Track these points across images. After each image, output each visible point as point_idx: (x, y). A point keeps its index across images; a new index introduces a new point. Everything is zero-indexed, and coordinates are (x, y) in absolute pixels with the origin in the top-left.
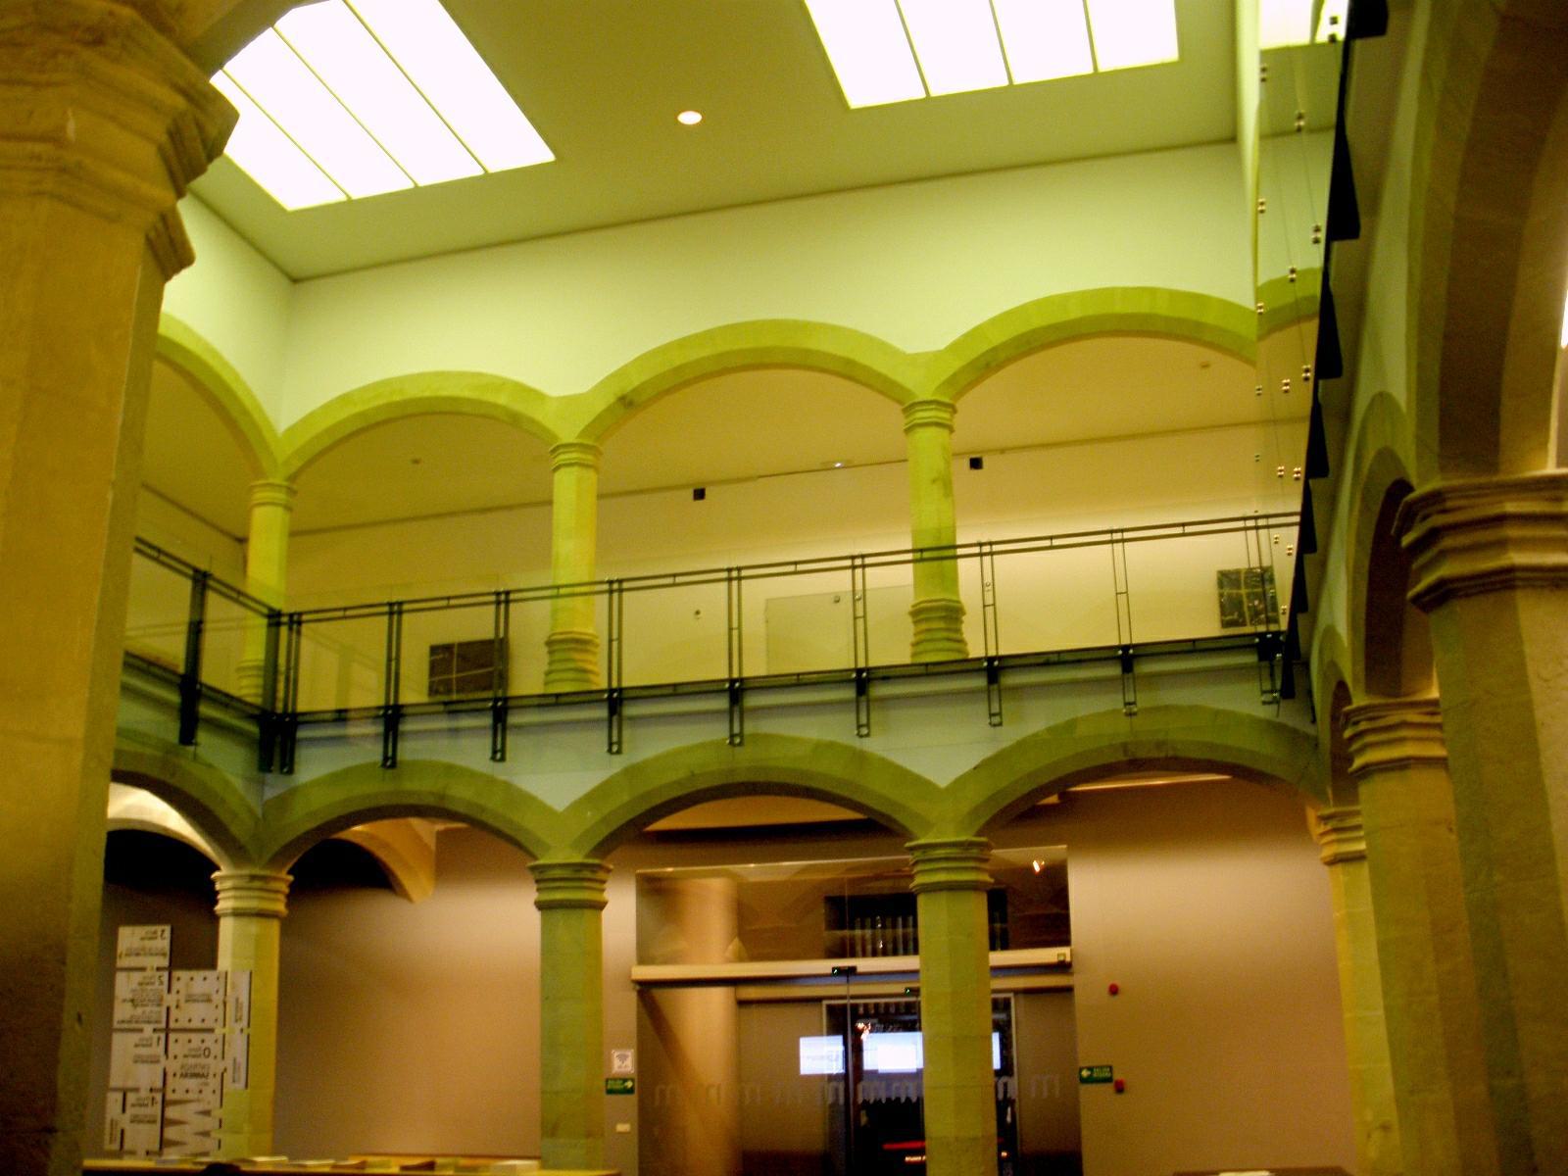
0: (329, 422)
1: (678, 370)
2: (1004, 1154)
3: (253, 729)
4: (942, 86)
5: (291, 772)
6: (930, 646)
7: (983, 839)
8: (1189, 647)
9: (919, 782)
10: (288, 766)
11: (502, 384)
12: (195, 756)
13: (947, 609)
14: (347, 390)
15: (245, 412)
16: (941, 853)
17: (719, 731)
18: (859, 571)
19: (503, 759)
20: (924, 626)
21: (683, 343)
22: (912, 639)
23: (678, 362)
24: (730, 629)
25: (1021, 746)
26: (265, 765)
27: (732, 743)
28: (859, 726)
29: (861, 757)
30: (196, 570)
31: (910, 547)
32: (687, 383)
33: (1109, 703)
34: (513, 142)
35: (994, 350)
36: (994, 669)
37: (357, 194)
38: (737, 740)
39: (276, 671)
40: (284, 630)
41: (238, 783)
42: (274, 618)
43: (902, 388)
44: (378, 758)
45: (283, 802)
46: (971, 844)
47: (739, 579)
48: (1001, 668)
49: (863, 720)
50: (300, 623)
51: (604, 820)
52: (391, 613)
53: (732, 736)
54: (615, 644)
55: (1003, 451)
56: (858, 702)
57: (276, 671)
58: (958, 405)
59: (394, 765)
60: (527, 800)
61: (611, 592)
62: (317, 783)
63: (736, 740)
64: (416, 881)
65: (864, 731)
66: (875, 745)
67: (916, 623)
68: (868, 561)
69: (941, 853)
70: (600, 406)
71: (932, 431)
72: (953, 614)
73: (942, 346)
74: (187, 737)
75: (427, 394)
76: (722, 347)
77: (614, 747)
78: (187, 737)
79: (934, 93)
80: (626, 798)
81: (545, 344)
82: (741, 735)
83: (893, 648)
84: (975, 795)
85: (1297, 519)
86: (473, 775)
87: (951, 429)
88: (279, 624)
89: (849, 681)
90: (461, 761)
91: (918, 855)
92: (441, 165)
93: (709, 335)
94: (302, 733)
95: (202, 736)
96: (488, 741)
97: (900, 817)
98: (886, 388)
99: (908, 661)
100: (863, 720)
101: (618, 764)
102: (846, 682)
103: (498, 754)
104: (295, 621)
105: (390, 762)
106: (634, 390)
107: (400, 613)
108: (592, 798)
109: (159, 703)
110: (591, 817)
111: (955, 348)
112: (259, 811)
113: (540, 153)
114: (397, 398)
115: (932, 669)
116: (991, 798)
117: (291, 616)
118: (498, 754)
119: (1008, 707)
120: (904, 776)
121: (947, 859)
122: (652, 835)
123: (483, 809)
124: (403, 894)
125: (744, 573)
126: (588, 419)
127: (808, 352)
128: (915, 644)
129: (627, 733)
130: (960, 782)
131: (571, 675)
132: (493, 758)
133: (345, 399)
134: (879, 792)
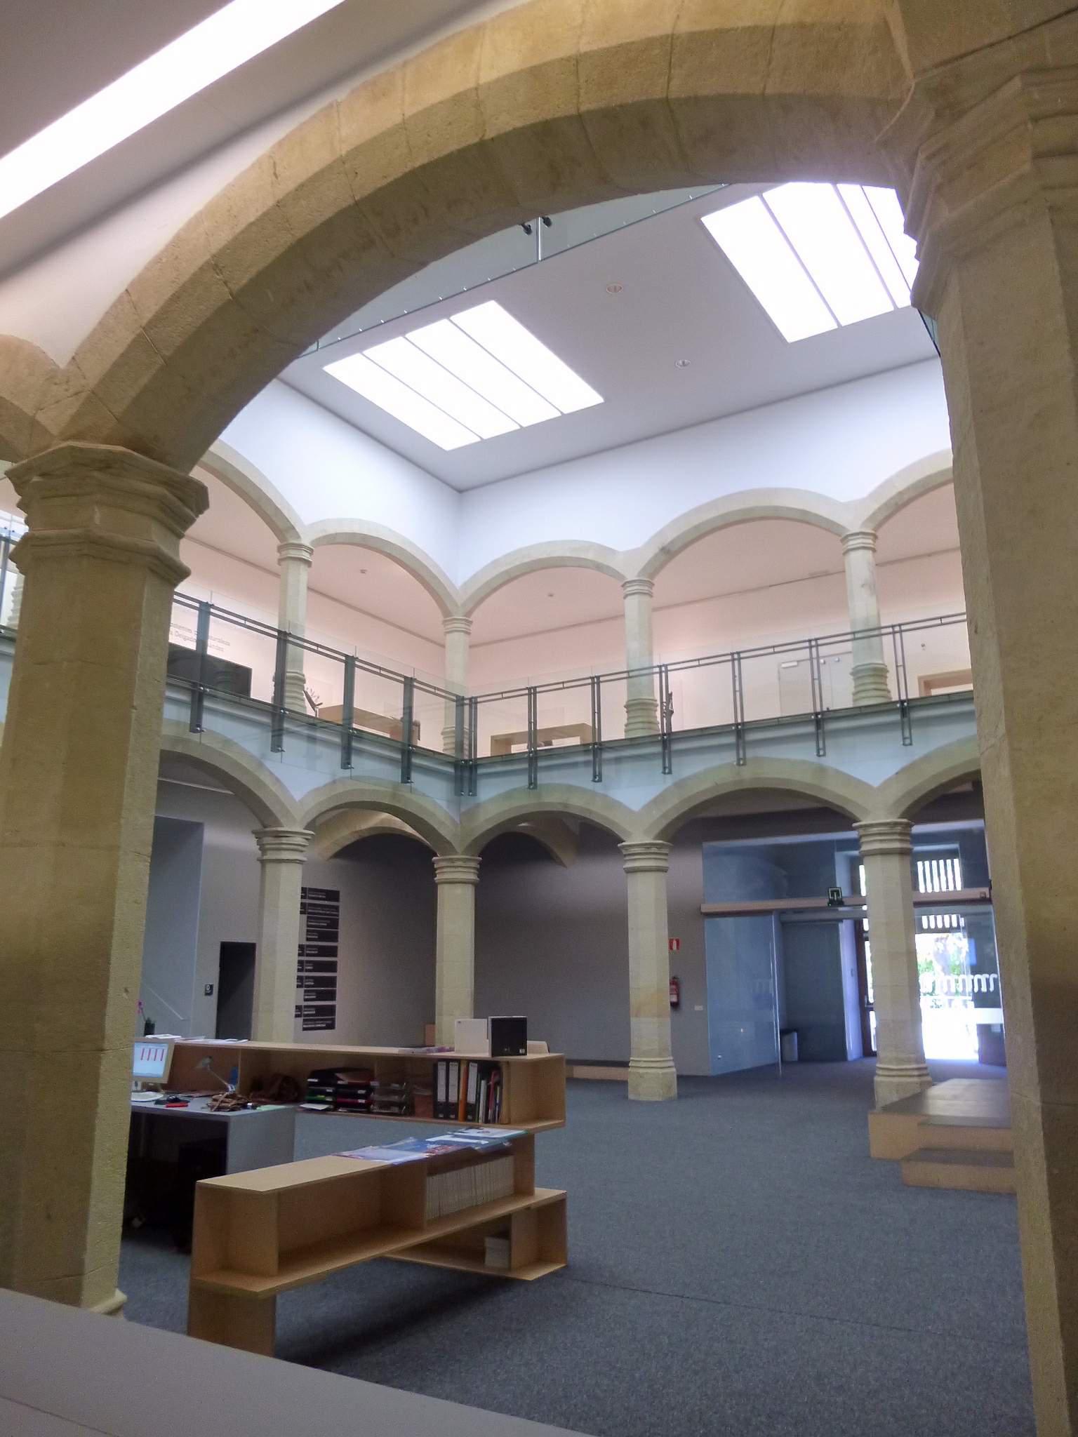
0: (485, 580)
1: (696, 527)
2: (698, 1008)
3: (451, 770)
4: (849, 317)
5: (475, 795)
6: (863, 694)
7: (905, 820)
8: (946, 699)
9: (859, 784)
10: (473, 791)
11: (590, 546)
12: (411, 790)
13: (875, 669)
14: (496, 557)
15: (435, 577)
16: (875, 830)
17: (522, 781)
18: (898, 636)
19: (600, 780)
20: (860, 682)
21: (698, 510)
22: (853, 690)
23: (696, 523)
24: (813, 679)
25: (927, 758)
26: (458, 791)
27: (739, 764)
28: (904, 739)
29: (822, 770)
30: (406, 678)
31: (849, 630)
32: (753, 520)
33: (730, 757)
34: (573, 393)
35: (900, 493)
36: (906, 708)
37: (567, 410)
38: (908, 741)
39: (463, 734)
40: (467, 708)
41: (443, 804)
42: (460, 701)
43: (839, 525)
44: (527, 783)
45: (469, 815)
46: (896, 824)
47: (901, 631)
48: (823, 720)
49: (907, 734)
50: (476, 703)
51: (664, 816)
52: (733, 660)
53: (739, 760)
54: (816, 682)
55: (929, 555)
56: (817, 735)
57: (463, 734)
58: (654, 581)
59: (535, 787)
60: (616, 805)
61: (733, 660)
62: (492, 800)
63: (741, 762)
64: (565, 857)
65: (908, 741)
66: (832, 760)
67: (855, 680)
68: (903, 628)
69: (875, 830)
70: (650, 554)
71: (861, 552)
72: (879, 673)
73: (865, 495)
74: (406, 778)
75: (545, 556)
76: (722, 511)
77: (667, 770)
78: (406, 778)
79: (844, 323)
80: (676, 801)
81: (616, 515)
82: (744, 759)
83: (840, 694)
84: (896, 792)
85: (965, 617)
86: (584, 791)
87: (651, 595)
88: (463, 705)
89: (811, 721)
90: (574, 782)
91: (862, 832)
92: (534, 413)
93: (713, 504)
94: (480, 771)
95: (415, 776)
96: (591, 770)
97: (850, 808)
98: (830, 527)
99: (851, 705)
100: (907, 734)
101: (669, 781)
102: (730, 732)
103: (597, 777)
104: (473, 702)
105: (533, 784)
106: (672, 542)
107: (739, 659)
108: (656, 802)
109: (391, 761)
110: (656, 814)
111: (872, 496)
112: (457, 820)
113: (597, 399)
114: (526, 560)
115: (864, 711)
116: (909, 793)
117: (470, 699)
118: (597, 777)
119: (916, 732)
120: (849, 779)
121: (880, 834)
122: (695, 827)
123: (590, 812)
124: (562, 864)
125: (820, 642)
126: (642, 565)
127: (776, 508)
128: (855, 694)
129: (674, 761)
130: (887, 784)
131: (640, 725)
132: (819, 755)
133: (495, 563)
134: (834, 791)
